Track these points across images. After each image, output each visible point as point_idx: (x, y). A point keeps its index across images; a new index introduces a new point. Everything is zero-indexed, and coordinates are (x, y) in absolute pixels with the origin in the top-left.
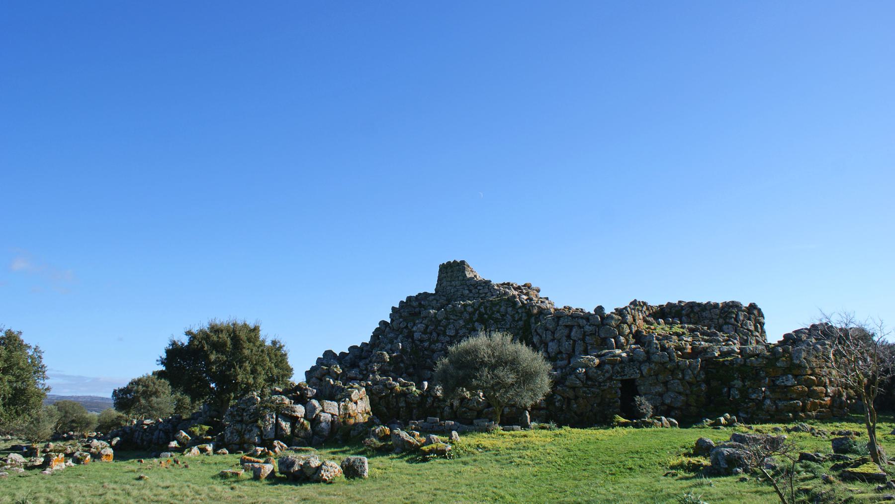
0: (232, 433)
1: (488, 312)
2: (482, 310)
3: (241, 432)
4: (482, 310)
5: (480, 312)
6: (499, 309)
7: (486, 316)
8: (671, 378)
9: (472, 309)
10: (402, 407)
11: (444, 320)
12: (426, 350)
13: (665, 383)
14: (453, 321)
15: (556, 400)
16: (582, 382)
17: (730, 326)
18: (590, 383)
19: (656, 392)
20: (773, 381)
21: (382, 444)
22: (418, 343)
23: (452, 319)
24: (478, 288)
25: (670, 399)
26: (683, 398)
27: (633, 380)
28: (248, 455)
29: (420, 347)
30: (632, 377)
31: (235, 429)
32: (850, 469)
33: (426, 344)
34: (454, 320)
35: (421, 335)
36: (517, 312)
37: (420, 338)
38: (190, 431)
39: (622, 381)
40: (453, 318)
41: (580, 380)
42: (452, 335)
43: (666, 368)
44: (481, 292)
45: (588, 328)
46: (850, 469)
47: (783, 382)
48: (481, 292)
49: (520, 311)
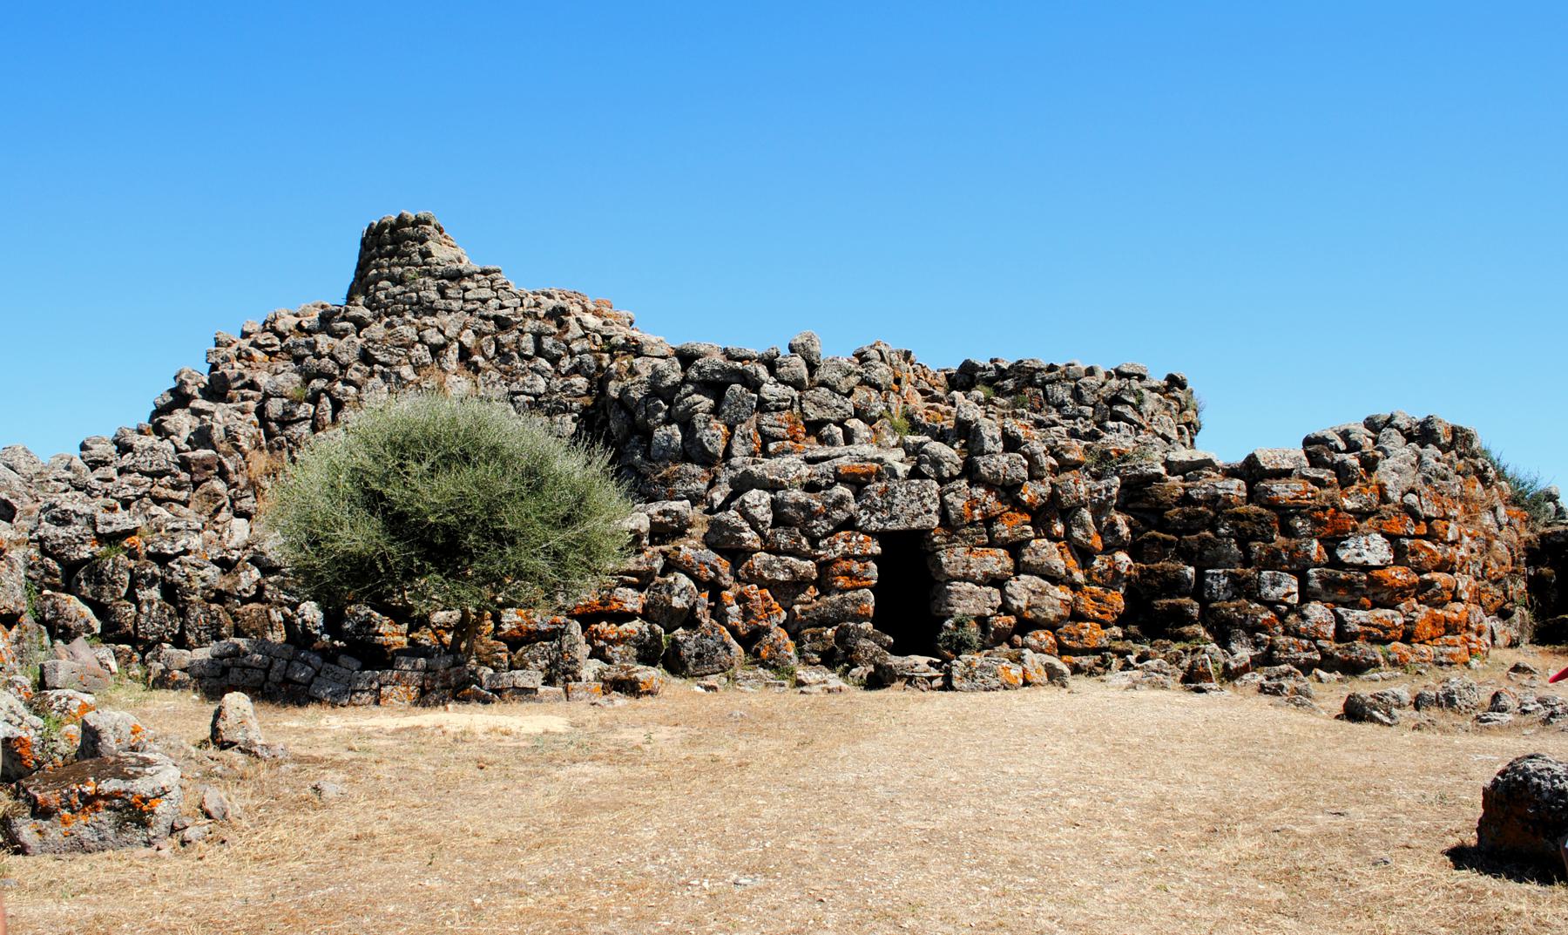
5: (461, 343)
8: (1032, 534)
10: (150, 603)
13: (1015, 548)
15: (677, 590)
16: (761, 534)
17: (1122, 423)
18: (783, 539)
19: (986, 575)
20: (1331, 551)
25: (1025, 596)
26: (1062, 595)
27: (923, 534)
30: (914, 525)
34: (385, 364)
39: (881, 536)
40: (382, 359)
41: (754, 527)
44: (469, 295)
45: (771, 390)
47: (1358, 555)
48: (469, 295)
49: (576, 347)
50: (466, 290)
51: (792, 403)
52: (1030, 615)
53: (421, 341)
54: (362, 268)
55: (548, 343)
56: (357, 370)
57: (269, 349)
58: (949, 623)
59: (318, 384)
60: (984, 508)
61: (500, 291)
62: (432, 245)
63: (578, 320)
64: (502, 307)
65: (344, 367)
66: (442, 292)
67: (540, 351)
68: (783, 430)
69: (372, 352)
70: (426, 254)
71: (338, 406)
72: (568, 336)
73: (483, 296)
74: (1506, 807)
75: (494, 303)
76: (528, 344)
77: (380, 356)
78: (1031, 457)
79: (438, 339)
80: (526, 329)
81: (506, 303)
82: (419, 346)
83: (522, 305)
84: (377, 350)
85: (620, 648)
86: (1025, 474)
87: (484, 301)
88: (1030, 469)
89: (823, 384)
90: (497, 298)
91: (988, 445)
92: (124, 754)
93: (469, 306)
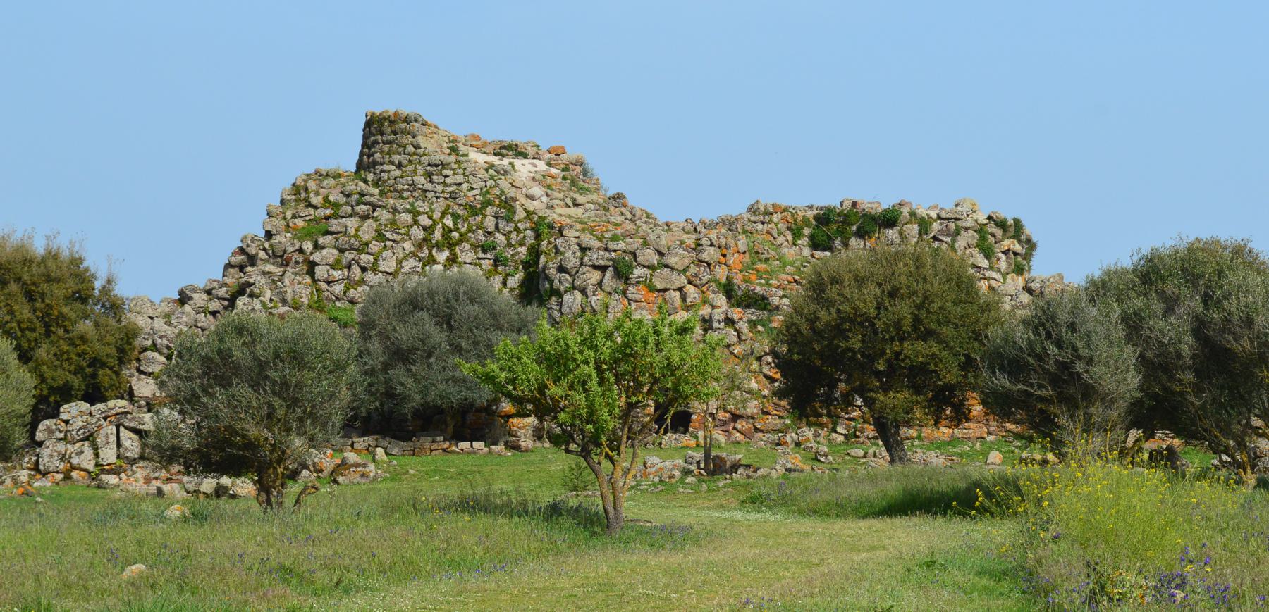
0: (51, 456)
1: (460, 226)
2: (449, 221)
3: (65, 455)
4: (449, 221)
5: (444, 225)
6: (482, 222)
7: (455, 234)
9: (430, 221)
11: (374, 242)
12: (338, 299)
14: (391, 243)
21: (1015, 388)
22: (324, 286)
23: (389, 240)
24: (446, 172)
28: (667, 425)
29: (326, 294)
31: (56, 451)
32: (1266, 404)
33: (338, 289)
34: (394, 241)
35: (328, 271)
36: (517, 229)
37: (326, 276)
38: (416, 413)
40: (391, 237)
42: (389, 271)
43: (732, 353)
44: (448, 181)
46: (1266, 404)
48: (448, 181)
50: (446, 176)
51: (646, 279)
52: (738, 412)
53: (416, 222)
54: (365, 138)
55: (502, 224)
56: (375, 245)
57: (307, 218)
58: (694, 417)
59: (349, 255)
60: (87, 356)
61: (470, 177)
62: (420, 140)
63: (522, 205)
64: (473, 189)
65: (367, 244)
66: (429, 175)
67: (497, 227)
68: (640, 296)
69: (385, 233)
70: (417, 147)
71: (364, 269)
72: (516, 218)
73: (458, 181)
74: (609, 418)
75: (465, 186)
76: (490, 223)
77: (389, 235)
78: (739, 332)
79: (427, 222)
80: (488, 213)
81: (474, 186)
82: (415, 227)
83: (486, 186)
84: (387, 231)
85: (524, 431)
86: (735, 339)
87: (460, 184)
88: (739, 337)
89: (667, 266)
90: (468, 182)
91: (715, 325)
92: (559, 258)
93: (450, 189)
